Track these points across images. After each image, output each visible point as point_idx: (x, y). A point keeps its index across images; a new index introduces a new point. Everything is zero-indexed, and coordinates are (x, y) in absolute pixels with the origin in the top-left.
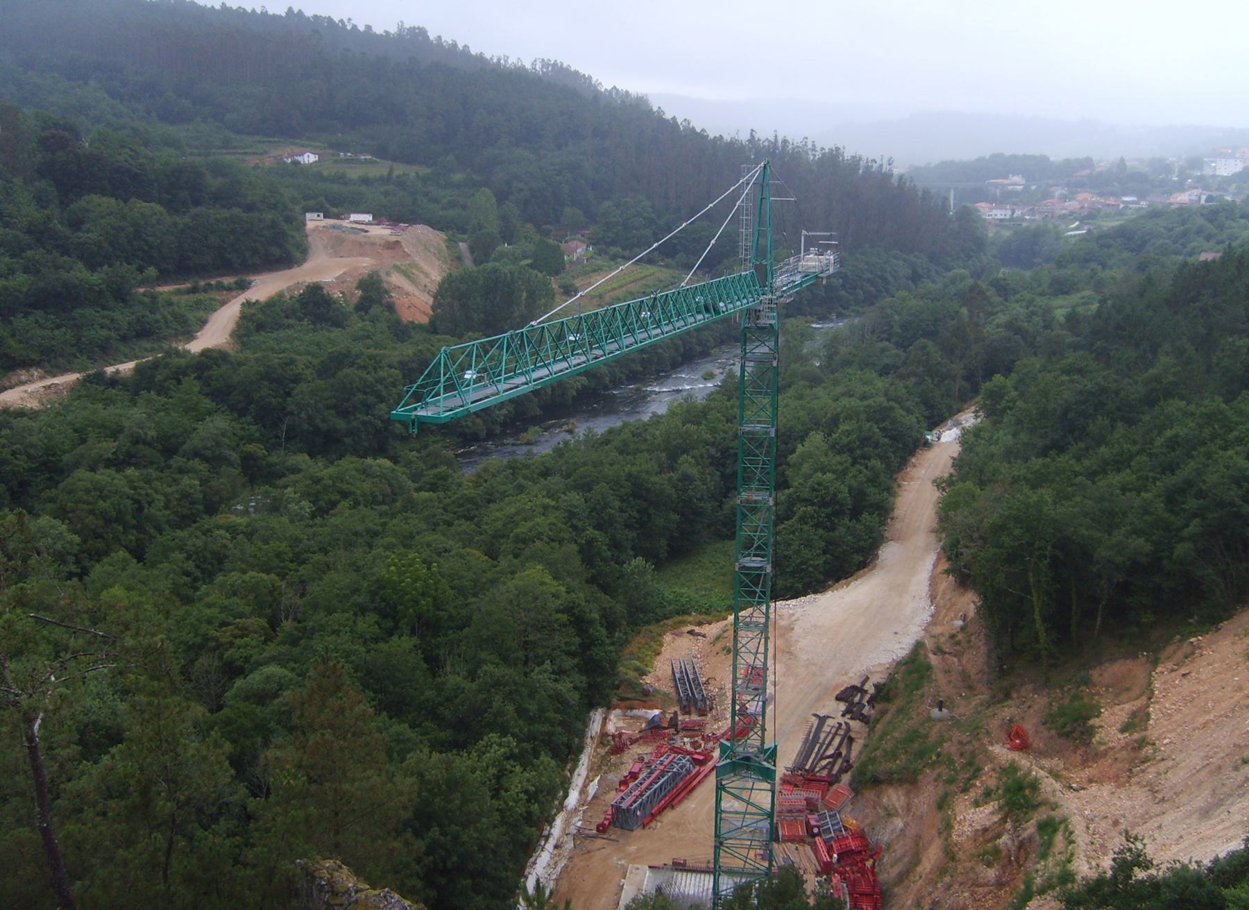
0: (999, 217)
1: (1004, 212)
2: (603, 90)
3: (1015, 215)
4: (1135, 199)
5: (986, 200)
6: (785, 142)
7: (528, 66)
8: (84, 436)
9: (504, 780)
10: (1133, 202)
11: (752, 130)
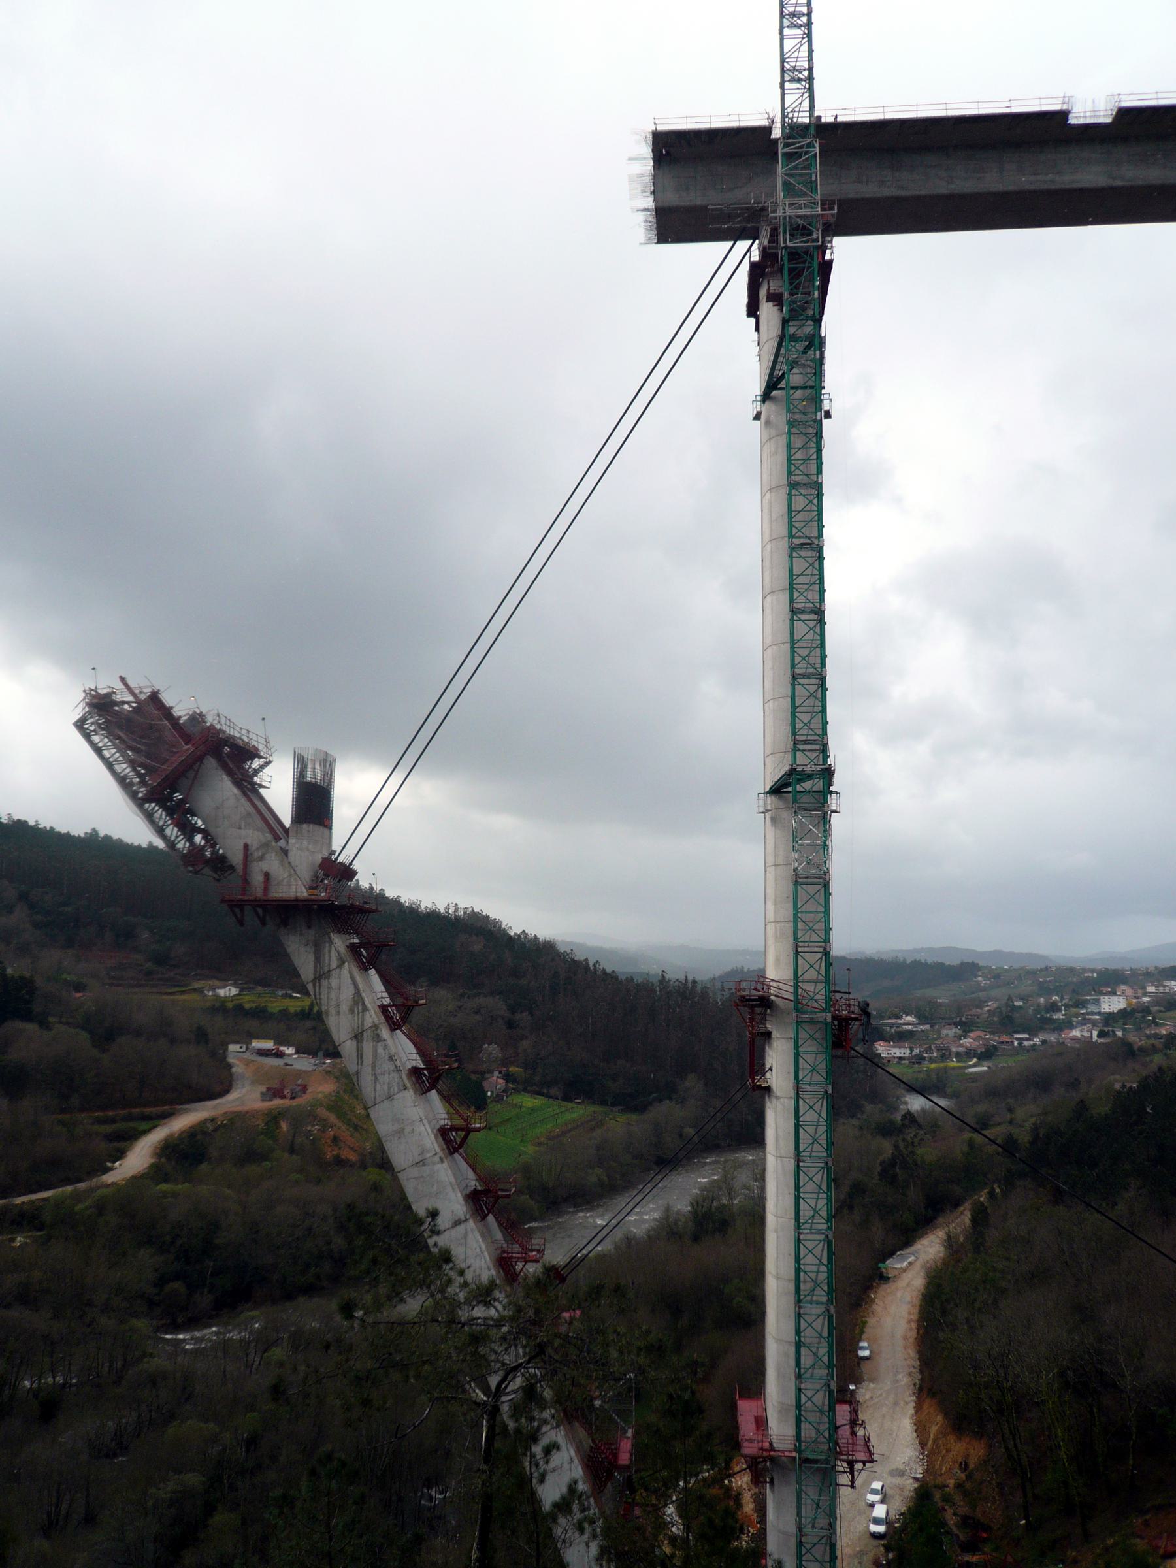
0: (898, 1055)
1: (903, 1050)
2: (512, 934)
3: (914, 1053)
4: (1027, 1036)
5: (883, 1039)
6: (695, 982)
7: (442, 911)
8: (839, 1052)
9: (293, 864)
10: (1027, 1039)
11: (663, 971)
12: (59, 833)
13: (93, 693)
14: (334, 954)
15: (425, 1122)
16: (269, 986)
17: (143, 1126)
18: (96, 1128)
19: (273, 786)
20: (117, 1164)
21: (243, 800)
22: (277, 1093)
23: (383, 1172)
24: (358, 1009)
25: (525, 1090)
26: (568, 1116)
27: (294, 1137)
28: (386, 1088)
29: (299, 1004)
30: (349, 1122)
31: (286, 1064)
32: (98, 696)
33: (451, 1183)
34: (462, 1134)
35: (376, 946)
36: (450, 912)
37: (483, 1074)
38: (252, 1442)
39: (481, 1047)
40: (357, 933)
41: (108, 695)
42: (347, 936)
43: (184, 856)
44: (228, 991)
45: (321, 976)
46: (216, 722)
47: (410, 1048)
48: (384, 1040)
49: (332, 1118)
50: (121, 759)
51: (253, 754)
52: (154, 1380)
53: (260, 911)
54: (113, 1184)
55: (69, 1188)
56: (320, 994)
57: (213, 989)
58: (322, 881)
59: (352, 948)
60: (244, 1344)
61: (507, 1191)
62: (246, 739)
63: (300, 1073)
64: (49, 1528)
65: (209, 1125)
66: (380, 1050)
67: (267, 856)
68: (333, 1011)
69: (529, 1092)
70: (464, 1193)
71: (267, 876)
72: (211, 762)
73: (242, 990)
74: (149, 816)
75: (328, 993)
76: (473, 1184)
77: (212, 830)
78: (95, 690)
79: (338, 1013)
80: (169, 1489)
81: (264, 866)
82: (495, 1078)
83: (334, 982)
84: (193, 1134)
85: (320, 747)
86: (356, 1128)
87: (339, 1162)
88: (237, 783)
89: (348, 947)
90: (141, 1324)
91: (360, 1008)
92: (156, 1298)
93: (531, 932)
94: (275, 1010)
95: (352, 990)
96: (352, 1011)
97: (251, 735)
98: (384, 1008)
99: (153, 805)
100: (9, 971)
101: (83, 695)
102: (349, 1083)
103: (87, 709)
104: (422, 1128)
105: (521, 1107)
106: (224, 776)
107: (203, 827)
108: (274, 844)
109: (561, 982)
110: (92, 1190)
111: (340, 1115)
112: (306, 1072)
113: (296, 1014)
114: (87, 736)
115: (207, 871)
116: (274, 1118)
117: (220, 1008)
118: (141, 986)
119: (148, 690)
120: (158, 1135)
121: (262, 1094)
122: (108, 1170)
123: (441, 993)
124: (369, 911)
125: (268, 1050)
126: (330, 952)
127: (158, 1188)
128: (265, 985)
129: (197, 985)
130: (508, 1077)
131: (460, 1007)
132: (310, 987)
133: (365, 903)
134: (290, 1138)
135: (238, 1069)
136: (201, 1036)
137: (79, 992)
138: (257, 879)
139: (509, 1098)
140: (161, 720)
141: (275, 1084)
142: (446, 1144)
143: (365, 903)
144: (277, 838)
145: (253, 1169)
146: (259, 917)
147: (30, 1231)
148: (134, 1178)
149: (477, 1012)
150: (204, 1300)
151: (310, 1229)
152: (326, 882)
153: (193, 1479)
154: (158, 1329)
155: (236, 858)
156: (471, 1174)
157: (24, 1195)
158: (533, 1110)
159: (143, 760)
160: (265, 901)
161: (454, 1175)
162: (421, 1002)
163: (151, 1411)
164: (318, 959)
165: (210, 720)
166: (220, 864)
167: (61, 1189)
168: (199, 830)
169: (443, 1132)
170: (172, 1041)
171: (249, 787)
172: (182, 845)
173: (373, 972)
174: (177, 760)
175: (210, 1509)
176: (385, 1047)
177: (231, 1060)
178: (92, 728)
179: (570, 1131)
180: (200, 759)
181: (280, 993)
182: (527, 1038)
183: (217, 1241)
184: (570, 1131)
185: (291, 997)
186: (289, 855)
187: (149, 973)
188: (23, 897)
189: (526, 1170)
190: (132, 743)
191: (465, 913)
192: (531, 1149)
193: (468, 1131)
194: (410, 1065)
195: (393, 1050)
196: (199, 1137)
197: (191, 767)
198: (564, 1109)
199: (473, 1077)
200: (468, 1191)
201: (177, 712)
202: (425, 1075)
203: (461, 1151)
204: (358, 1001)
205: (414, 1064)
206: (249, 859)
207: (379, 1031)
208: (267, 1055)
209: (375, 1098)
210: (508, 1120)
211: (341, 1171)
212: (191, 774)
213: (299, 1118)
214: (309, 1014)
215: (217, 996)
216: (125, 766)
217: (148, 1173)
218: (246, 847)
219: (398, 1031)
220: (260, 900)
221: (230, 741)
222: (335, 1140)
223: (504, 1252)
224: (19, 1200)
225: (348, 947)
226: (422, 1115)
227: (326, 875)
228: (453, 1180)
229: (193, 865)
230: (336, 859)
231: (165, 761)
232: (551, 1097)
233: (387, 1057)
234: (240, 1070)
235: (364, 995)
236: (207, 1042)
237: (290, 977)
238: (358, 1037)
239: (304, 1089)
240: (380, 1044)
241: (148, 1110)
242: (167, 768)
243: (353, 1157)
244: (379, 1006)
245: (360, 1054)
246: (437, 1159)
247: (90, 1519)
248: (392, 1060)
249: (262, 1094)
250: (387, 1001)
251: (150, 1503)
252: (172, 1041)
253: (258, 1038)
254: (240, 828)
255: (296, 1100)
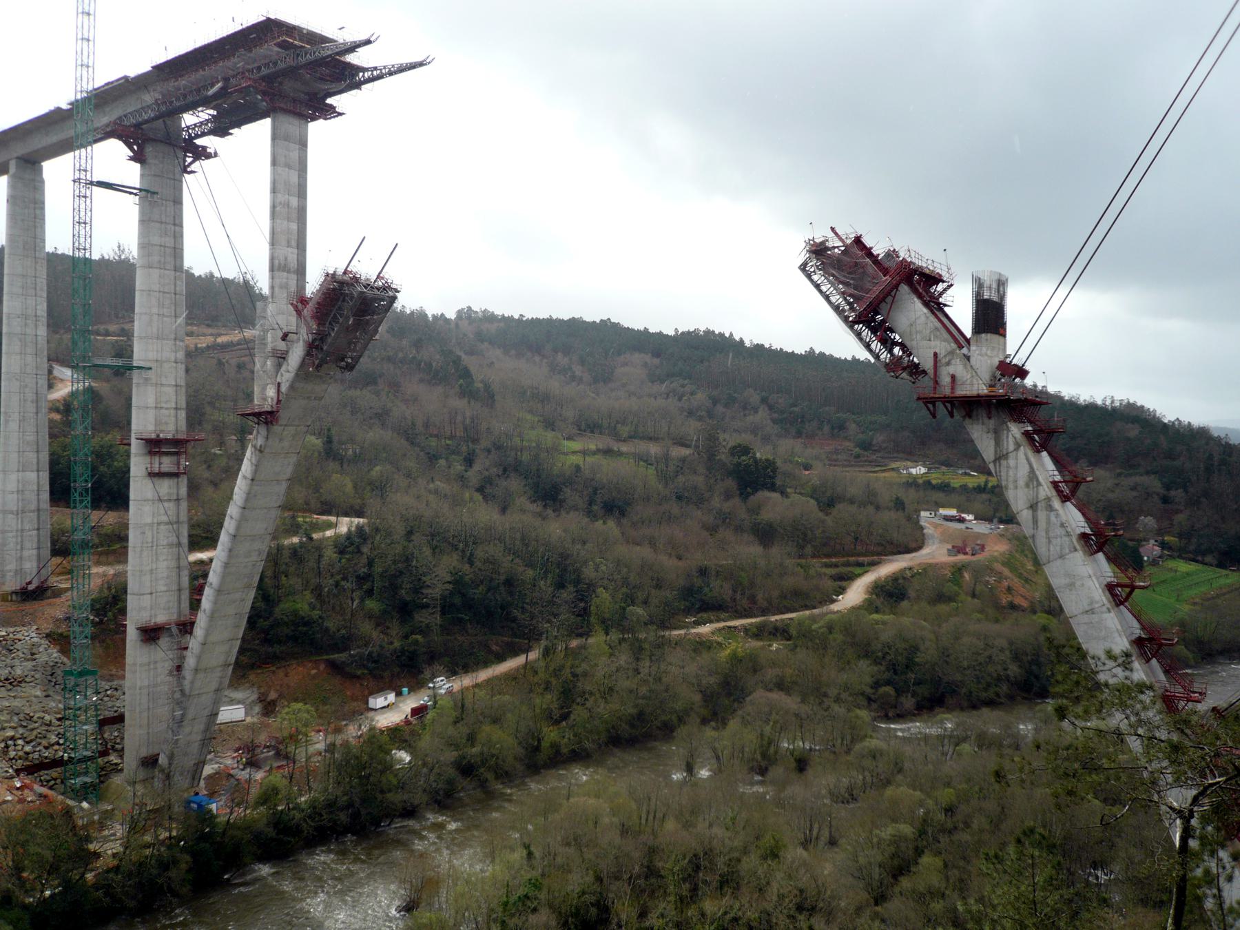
2: (1166, 421)
12: (786, 352)
13: (811, 242)
14: (1011, 440)
15: (1094, 578)
16: (952, 466)
17: (858, 570)
18: (824, 570)
19: (954, 304)
20: (840, 597)
21: (932, 318)
22: (960, 550)
23: (1051, 617)
24: (1033, 484)
25: (1180, 557)
26: (1223, 581)
27: (975, 585)
28: (1058, 548)
29: (976, 480)
30: (1020, 576)
31: (967, 528)
32: (815, 244)
33: (1117, 630)
34: (1127, 590)
35: (1048, 433)
36: (1107, 404)
37: (1140, 542)
38: (949, 810)
39: (1137, 518)
40: (1030, 422)
41: (823, 243)
42: (1022, 425)
43: (886, 365)
44: (919, 470)
45: (1000, 457)
46: (907, 256)
47: (1078, 516)
48: (1056, 510)
49: (1006, 572)
50: (835, 292)
51: (937, 279)
52: (874, 755)
53: (948, 405)
54: (838, 612)
55: (807, 612)
56: (1000, 472)
57: (907, 468)
58: (999, 380)
59: (1027, 434)
60: (941, 738)
61: (1169, 640)
62: (931, 268)
63: (979, 535)
64: (805, 844)
65: (907, 572)
66: (1053, 518)
67: (953, 362)
68: (1011, 486)
69: (1183, 559)
70: (1130, 639)
71: (953, 377)
72: (904, 288)
73: (929, 469)
74: (858, 335)
75: (1008, 471)
76: (1138, 632)
77: (908, 343)
78: (813, 240)
79: (1016, 487)
80: (888, 833)
81: (951, 369)
82: (1150, 545)
83: (1012, 462)
84: (895, 578)
85: (994, 270)
86: (1027, 580)
87: (1013, 607)
88: (926, 304)
89: (1023, 434)
90: (864, 714)
91: (1035, 483)
92: (873, 696)
93: (1185, 419)
94: (957, 485)
95: (1027, 467)
96: (1027, 485)
97: (935, 264)
98: (1055, 484)
99: (861, 325)
100: (758, 455)
101: (805, 244)
102: (1023, 545)
103: (808, 255)
104: (1091, 583)
105: (1176, 571)
106: (916, 299)
107: (900, 341)
108: (958, 351)
109: (1216, 464)
110: (823, 615)
111: (1013, 569)
112: (984, 534)
113: (974, 489)
114: (809, 276)
115: (904, 375)
116: (959, 570)
117: (913, 483)
118: (852, 466)
119: (853, 236)
120: (869, 578)
121: (948, 550)
122: (833, 601)
123: (1100, 472)
124: (1041, 404)
125: (953, 516)
126: (1007, 437)
127: (872, 616)
128: (946, 466)
129: (894, 465)
130: (1163, 545)
131: (1117, 485)
132: (991, 466)
133: (1037, 397)
134: (972, 585)
135: (929, 531)
136: (899, 505)
137: (808, 470)
138: (945, 380)
139: (1165, 563)
140: (864, 258)
141: (960, 544)
142: (1113, 598)
143: (1037, 397)
144: (961, 347)
145: (943, 608)
146: (948, 410)
147: (782, 640)
148: (853, 608)
149: (1133, 488)
150: (908, 702)
151: (990, 657)
152: (1003, 380)
153: (906, 829)
154: (875, 719)
155: (928, 365)
156: (1136, 624)
157: (777, 614)
158: (1188, 574)
159: (851, 291)
160: (952, 397)
161: (1121, 623)
162: (1088, 479)
163: (872, 776)
164: (998, 443)
165: (903, 255)
166: (915, 370)
167: (801, 613)
168: (897, 344)
169: (1110, 588)
170: (878, 508)
171: (935, 306)
172: (885, 356)
173: (1045, 454)
174: (876, 290)
175: (919, 852)
176: (1057, 516)
177: (922, 523)
178: (812, 270)
179: (1224, 594)
180: (896, 287)
181: (960, 472)
182: (1181, 511)
183: (917, 660)
184: (1224, 594)
185: (970, 475)
186: (971, 360)
187: (858, 456)
188: (764, 400)
189: (1182, 624)
190: (842, 279)
191: (1121, 404)
192: (1186, 608)
193: (1133, 588)
194: (1079, 531)
195: (1064, 518)
196: (901, 581)
197: (889, 294)
198: (1218, 575)
199: (1130, 543)
200: (1134, 637)
201: (875, 252)
202: (1093, 540)
203: (1126, 604)
204: (1032, 477)
205: (1082, 530)
206: (938, 365)
207: (1051, 503)
208: (951, 521)
209: (1049, 556)
210: (1163, 582)
211: (1015, 614)
212: (889, 299)
213: (979, 571)
214: (985, 488)
215: (910, 474)
216: (838, 297)
217: (863, 606)
218: (935, 355)
219: (1068, 503)
220: (948, 397)
221: (919, 271)
222: (1009, 589)
223: (1167, 691)
224: (773, 618)
225: (1023, 434)
226: (1091, 572)
227: (1003, 375)
228: (1119, 627)
229: (894, 372)
230: (1011, 362)
231: (868, 291)
232: (1206, 564)
233: (1059, 525)
234: (930, 532)
235: (1038, 473)
236: (904, 509)
237: (972, 458)
238: (1033, 507)
239: (983, 548)
240: (1052, 513)
241: (861, 559)
242: (871, 296)
243: (1025, 604)
244: (1051, 482)
245: (1035, 521)
246: (1104, 609)
247: (832, 842)
248: (1064, 527)
249: (948, 550)
250: (1058, 478)
251: (875, 840)
252: (878, 508)
253: (943, 507)
254: (930, 340)
255: (977, 556)
